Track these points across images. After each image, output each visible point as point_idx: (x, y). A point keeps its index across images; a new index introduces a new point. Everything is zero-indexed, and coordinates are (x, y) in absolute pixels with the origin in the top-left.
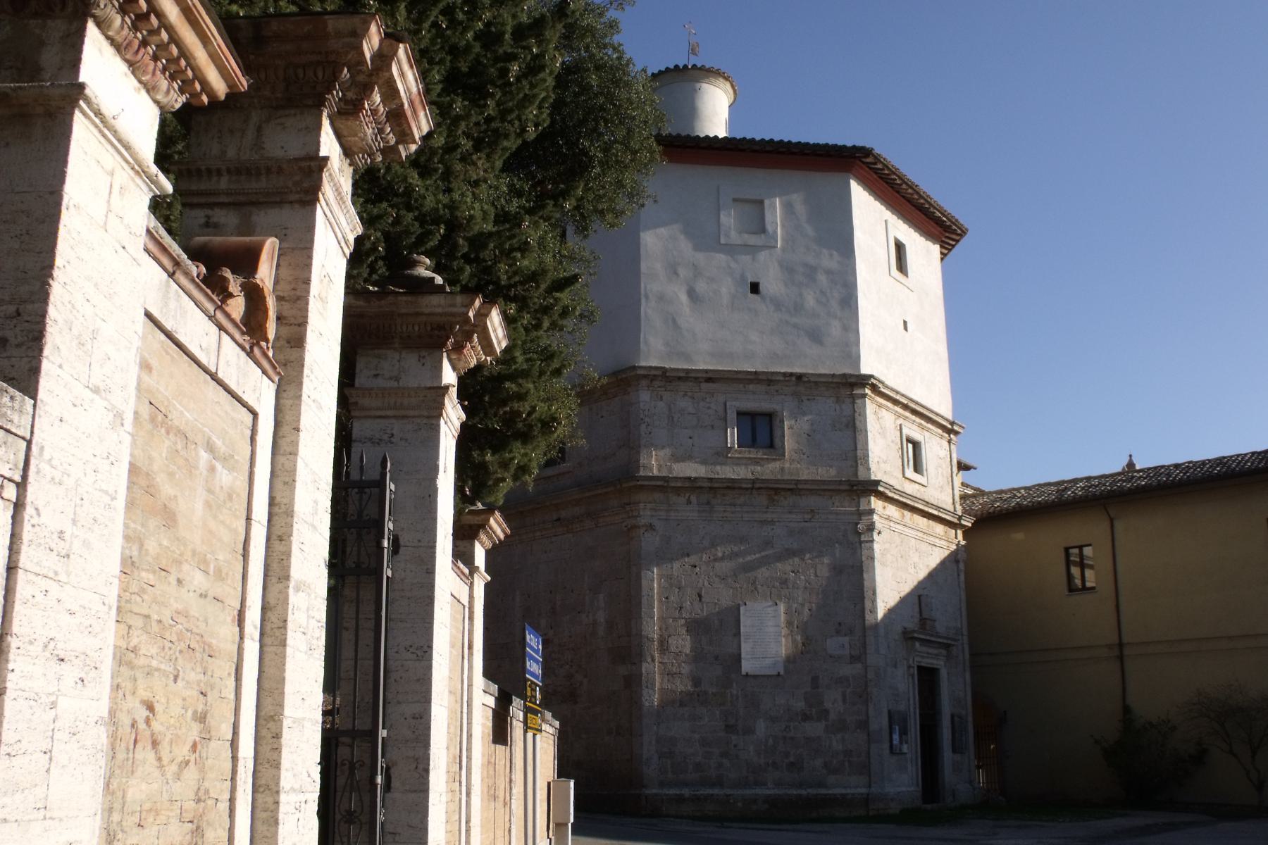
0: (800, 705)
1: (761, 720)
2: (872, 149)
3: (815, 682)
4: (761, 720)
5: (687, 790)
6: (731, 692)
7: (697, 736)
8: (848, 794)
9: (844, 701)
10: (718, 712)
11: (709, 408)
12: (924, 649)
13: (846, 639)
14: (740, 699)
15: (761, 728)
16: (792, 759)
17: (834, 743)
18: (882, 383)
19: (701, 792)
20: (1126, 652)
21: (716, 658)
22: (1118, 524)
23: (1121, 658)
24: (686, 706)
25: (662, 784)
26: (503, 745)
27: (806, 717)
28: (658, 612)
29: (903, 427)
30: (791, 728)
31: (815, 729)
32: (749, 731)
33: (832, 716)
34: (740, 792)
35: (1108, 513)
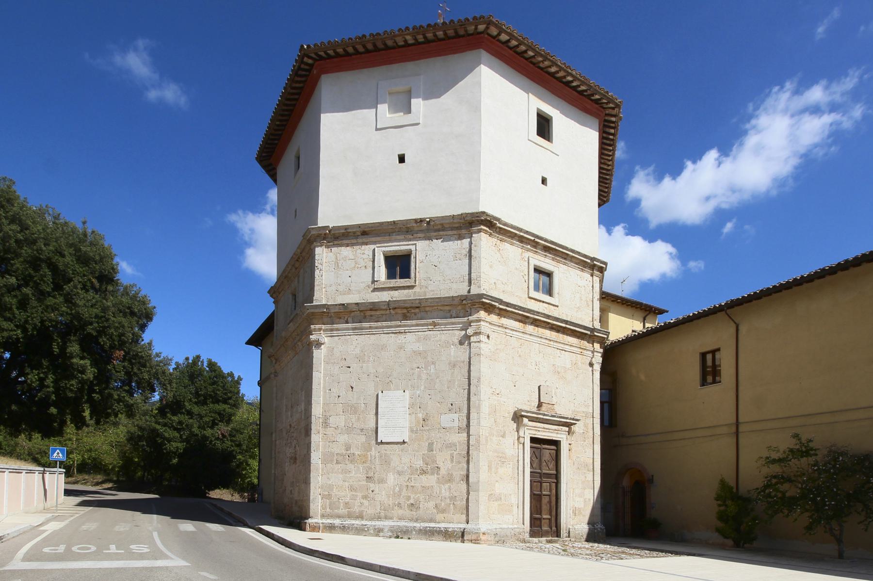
0: (419, 463)
1: (391, 473)
2: (674, 179)
3: (431, 445)
4: (391, 473)
5: (338, 520)
6: (370, 454)
7: (347, 484)
8: (449, 528)
9: (452, 461)
10: (361, 468)
11: (363, 254)
12: (531, 423)
13: (457, 415)
14: (377, 459)
15: (391, 479)
16: (412, 501)
17: (443, 491)
18: (498, 220)
19: (347, 522)
20: (741, 429)
21: (362, 430)
22: (743, 329)
23: (737, 433)
24: (340, 463)
25: (323, 516)
26: (586, 539)
27: (424, 472)
28: (323, 400)
29: (530, 258)
30: (413, 479)
31: (430, 480)
32: (382, 481)
33: (443, 471)
34: (373, 523)
35: (733, 320)
